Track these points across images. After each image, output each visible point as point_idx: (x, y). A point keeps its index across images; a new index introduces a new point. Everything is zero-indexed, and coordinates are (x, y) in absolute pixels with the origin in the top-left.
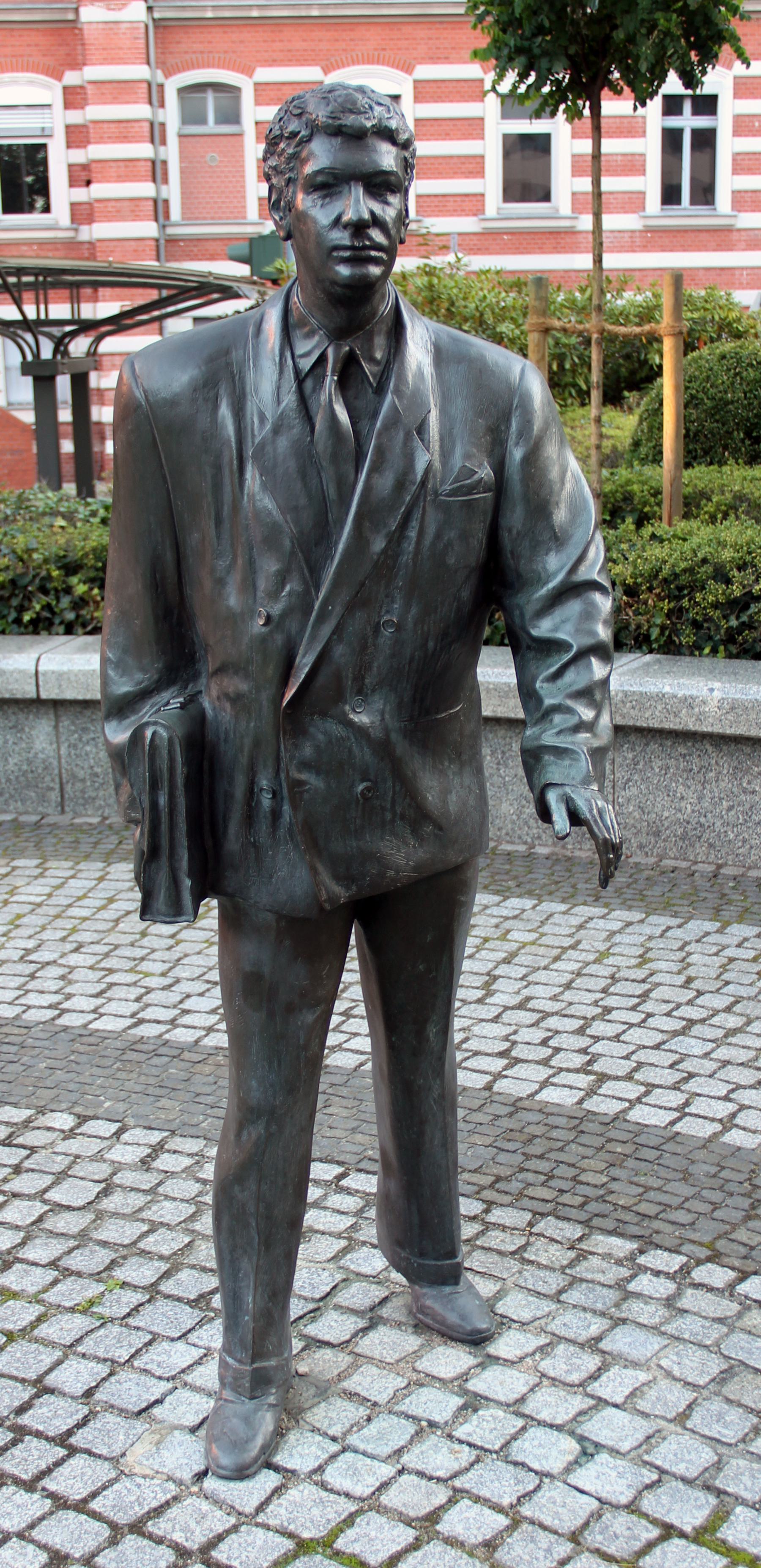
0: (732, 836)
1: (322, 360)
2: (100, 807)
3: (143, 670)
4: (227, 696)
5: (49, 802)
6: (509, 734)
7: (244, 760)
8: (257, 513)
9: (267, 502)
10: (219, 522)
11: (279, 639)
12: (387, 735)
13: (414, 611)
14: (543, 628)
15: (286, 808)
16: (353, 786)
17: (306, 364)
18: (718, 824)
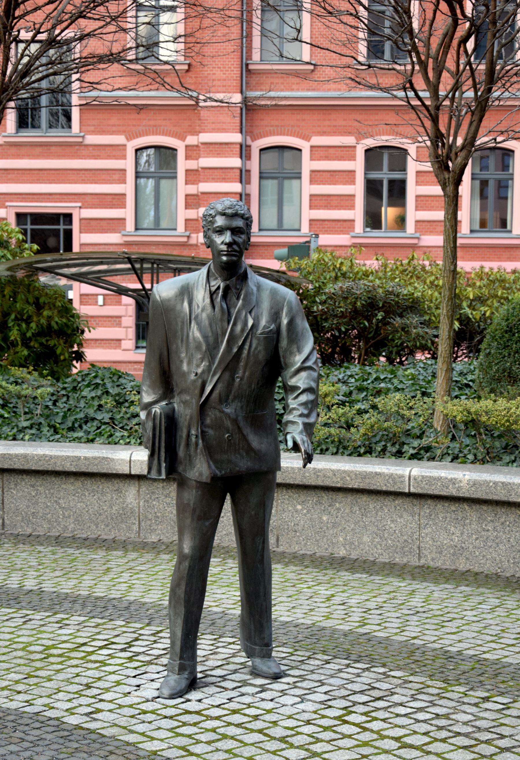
0: (477, 553)
1: (219, 288)
2: (159, 534)
3: (155, 394)
4: (182, 402)
5: (132, 530)
6: (368, 499)
7: (186, 423)
8: (194, 338)
9: (197, 334)
10: (182, 341)
11: (200, 381)
12: (237, 416)
13: (247, 374)
14: (292, 382)
15: (200, 441)
16: (224, 435)
17: (213, 289)
18: (471, 547)
